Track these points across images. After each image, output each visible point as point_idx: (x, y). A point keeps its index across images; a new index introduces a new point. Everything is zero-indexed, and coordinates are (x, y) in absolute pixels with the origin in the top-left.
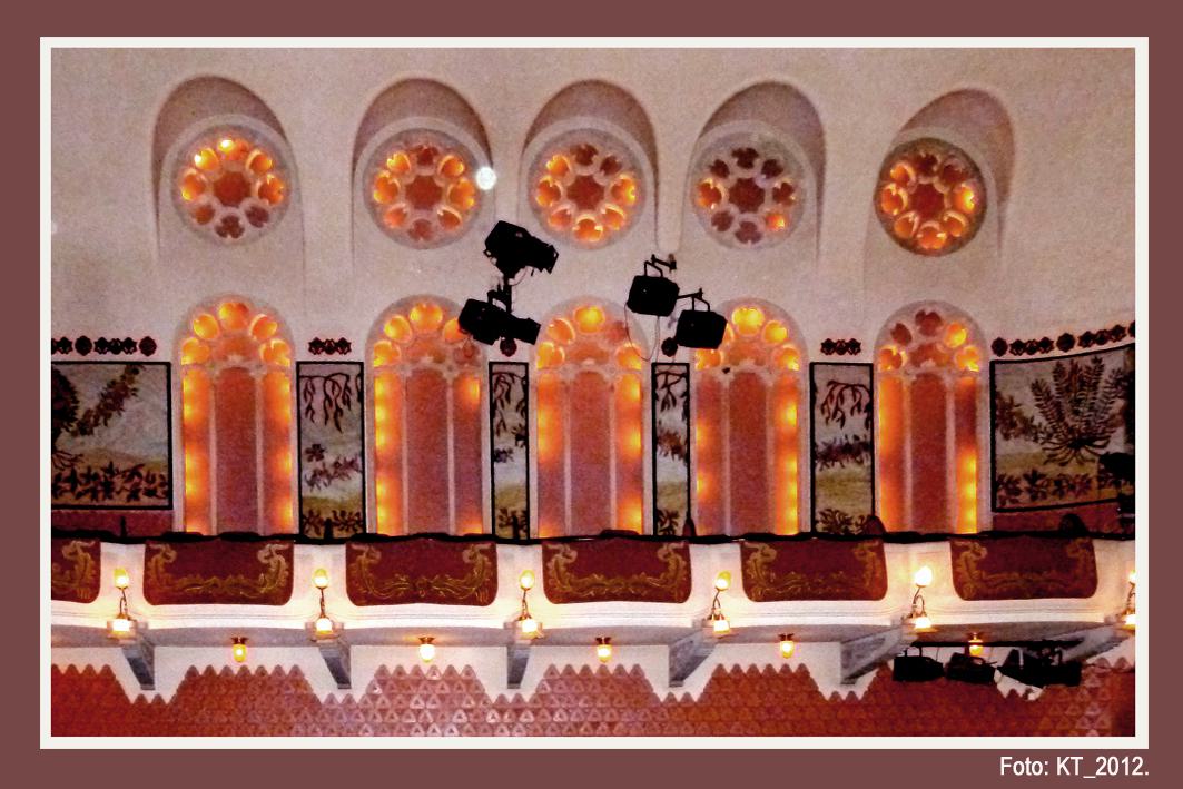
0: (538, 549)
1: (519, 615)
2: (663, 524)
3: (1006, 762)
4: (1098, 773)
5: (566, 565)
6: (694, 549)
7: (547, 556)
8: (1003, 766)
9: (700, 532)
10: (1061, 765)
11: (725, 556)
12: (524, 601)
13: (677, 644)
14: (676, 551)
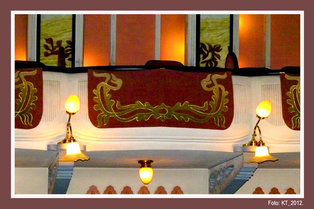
0: (85, 76)
1: (63, 138)
2: (205, 56)
3: (269, 202)
4: (291, 205)
5: (111, 92)
6: (236, 80)
7: (92, 84)
8: (269, 203)
9: (241, 65)
10: (283, 203)
11: (267, 88)
12: (69, 125)
13: (217, 168)
14: (219, 81)
